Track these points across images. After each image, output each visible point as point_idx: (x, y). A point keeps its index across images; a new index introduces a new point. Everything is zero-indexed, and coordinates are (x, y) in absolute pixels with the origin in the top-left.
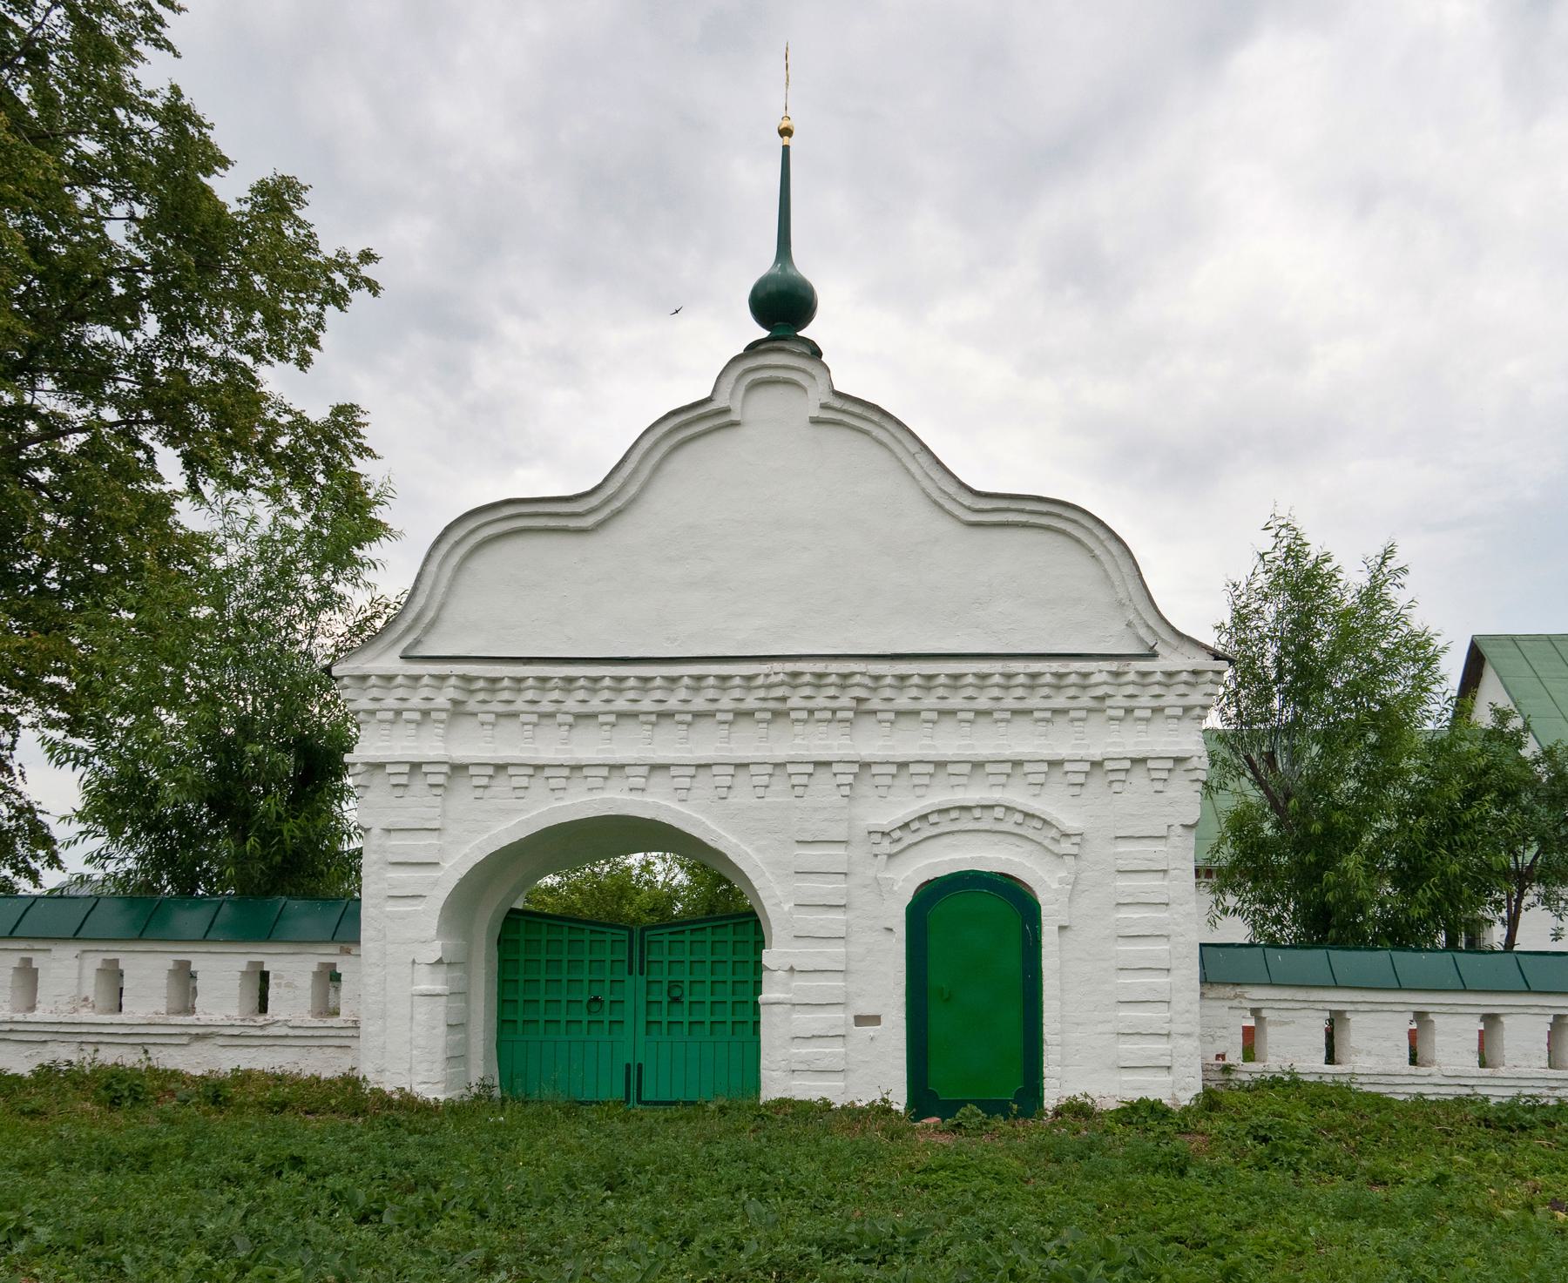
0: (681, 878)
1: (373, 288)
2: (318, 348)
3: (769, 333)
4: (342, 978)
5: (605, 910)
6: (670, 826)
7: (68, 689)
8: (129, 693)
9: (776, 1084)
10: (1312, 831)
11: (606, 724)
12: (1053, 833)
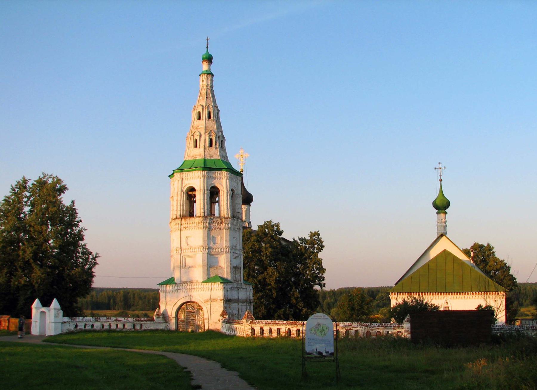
1: (81, 221)
2: (94, 272)
5: (283, 268)
6: (286, 239)
7: (59, 251)
8: (46, 230)
11: (177, 213)
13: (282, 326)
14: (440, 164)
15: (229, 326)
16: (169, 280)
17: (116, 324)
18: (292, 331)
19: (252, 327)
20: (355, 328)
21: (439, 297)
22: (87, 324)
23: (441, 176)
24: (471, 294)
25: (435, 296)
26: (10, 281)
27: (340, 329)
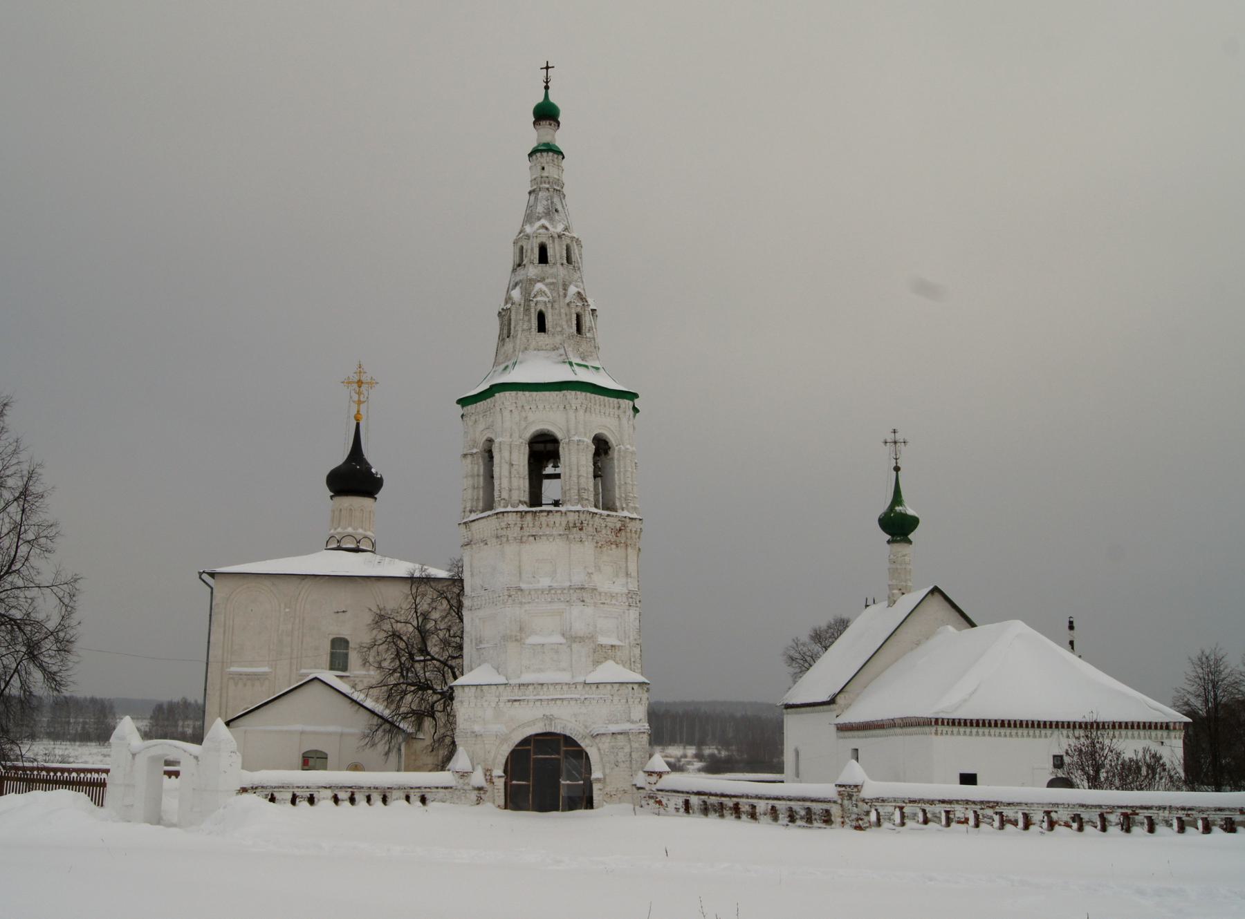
14: (895, 432)
17: (367, 794)
18: (981, 817)
21: (1042, 732)
22: (298, 794)
23: (896, 459)
25: (1033, 729)
27: (1107, 813)
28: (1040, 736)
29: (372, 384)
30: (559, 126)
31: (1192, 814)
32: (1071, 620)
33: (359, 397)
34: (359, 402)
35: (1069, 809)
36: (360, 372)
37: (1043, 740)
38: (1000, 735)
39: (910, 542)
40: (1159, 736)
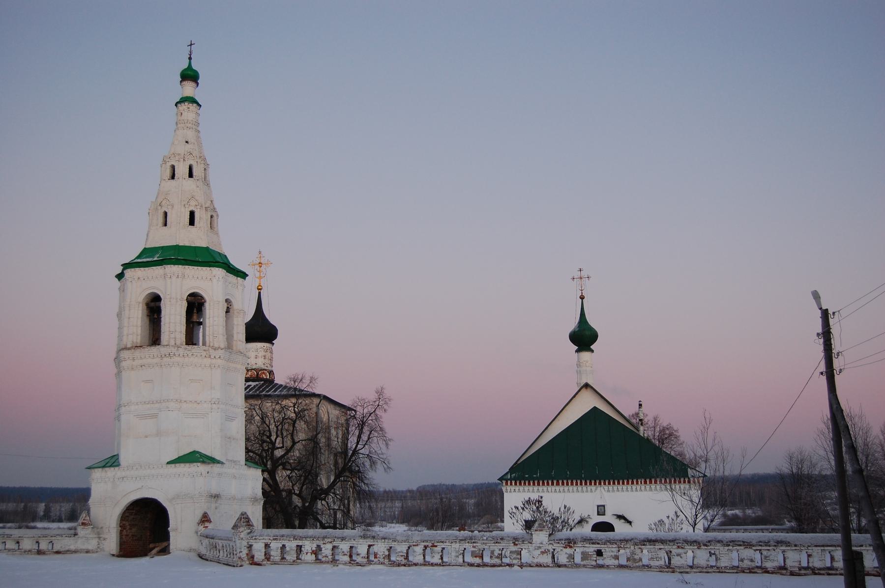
0: (300, 505)
3: (577, 347)
4: (286, 546)
9: (591, 347)
10: (742, 514)
12: (239, 565)
13: (306, 542)
14: (580, 271)
15: (211, 542)
16: (108, 460)
19: (250, 544)
20: (442, 544)
23: (582, 290)
24: (643, 483)
26: (881, 520)
28: (587, 491)
29: (268, 263)
30: (198, 85)
31: (478, 546)
32: (641, 403)
33: (260, 274)
34: (260, 278)
35: (386, 543)
36: (260, 257)
37: (589, 494)
38: (555, 491)
39: (592, 351)
40: (682, 488)
